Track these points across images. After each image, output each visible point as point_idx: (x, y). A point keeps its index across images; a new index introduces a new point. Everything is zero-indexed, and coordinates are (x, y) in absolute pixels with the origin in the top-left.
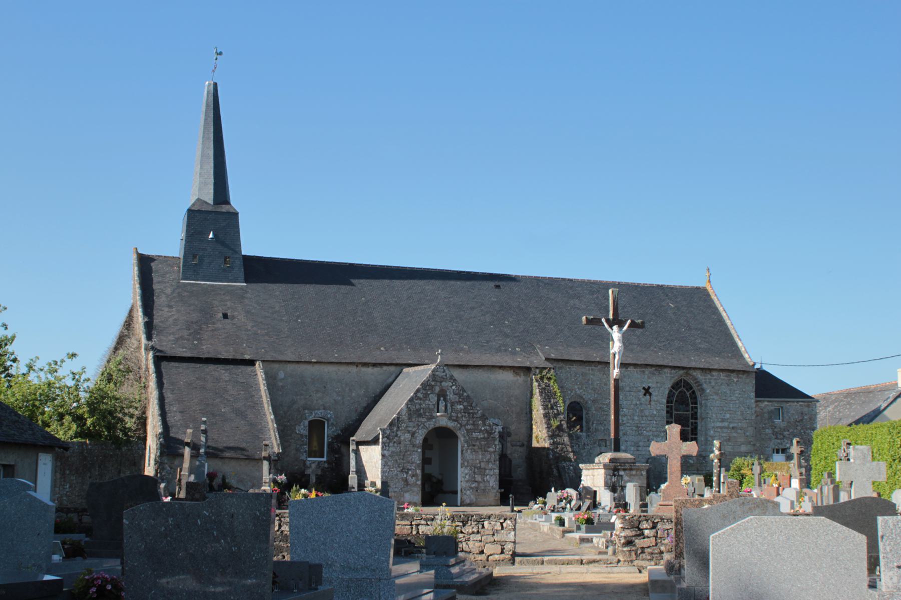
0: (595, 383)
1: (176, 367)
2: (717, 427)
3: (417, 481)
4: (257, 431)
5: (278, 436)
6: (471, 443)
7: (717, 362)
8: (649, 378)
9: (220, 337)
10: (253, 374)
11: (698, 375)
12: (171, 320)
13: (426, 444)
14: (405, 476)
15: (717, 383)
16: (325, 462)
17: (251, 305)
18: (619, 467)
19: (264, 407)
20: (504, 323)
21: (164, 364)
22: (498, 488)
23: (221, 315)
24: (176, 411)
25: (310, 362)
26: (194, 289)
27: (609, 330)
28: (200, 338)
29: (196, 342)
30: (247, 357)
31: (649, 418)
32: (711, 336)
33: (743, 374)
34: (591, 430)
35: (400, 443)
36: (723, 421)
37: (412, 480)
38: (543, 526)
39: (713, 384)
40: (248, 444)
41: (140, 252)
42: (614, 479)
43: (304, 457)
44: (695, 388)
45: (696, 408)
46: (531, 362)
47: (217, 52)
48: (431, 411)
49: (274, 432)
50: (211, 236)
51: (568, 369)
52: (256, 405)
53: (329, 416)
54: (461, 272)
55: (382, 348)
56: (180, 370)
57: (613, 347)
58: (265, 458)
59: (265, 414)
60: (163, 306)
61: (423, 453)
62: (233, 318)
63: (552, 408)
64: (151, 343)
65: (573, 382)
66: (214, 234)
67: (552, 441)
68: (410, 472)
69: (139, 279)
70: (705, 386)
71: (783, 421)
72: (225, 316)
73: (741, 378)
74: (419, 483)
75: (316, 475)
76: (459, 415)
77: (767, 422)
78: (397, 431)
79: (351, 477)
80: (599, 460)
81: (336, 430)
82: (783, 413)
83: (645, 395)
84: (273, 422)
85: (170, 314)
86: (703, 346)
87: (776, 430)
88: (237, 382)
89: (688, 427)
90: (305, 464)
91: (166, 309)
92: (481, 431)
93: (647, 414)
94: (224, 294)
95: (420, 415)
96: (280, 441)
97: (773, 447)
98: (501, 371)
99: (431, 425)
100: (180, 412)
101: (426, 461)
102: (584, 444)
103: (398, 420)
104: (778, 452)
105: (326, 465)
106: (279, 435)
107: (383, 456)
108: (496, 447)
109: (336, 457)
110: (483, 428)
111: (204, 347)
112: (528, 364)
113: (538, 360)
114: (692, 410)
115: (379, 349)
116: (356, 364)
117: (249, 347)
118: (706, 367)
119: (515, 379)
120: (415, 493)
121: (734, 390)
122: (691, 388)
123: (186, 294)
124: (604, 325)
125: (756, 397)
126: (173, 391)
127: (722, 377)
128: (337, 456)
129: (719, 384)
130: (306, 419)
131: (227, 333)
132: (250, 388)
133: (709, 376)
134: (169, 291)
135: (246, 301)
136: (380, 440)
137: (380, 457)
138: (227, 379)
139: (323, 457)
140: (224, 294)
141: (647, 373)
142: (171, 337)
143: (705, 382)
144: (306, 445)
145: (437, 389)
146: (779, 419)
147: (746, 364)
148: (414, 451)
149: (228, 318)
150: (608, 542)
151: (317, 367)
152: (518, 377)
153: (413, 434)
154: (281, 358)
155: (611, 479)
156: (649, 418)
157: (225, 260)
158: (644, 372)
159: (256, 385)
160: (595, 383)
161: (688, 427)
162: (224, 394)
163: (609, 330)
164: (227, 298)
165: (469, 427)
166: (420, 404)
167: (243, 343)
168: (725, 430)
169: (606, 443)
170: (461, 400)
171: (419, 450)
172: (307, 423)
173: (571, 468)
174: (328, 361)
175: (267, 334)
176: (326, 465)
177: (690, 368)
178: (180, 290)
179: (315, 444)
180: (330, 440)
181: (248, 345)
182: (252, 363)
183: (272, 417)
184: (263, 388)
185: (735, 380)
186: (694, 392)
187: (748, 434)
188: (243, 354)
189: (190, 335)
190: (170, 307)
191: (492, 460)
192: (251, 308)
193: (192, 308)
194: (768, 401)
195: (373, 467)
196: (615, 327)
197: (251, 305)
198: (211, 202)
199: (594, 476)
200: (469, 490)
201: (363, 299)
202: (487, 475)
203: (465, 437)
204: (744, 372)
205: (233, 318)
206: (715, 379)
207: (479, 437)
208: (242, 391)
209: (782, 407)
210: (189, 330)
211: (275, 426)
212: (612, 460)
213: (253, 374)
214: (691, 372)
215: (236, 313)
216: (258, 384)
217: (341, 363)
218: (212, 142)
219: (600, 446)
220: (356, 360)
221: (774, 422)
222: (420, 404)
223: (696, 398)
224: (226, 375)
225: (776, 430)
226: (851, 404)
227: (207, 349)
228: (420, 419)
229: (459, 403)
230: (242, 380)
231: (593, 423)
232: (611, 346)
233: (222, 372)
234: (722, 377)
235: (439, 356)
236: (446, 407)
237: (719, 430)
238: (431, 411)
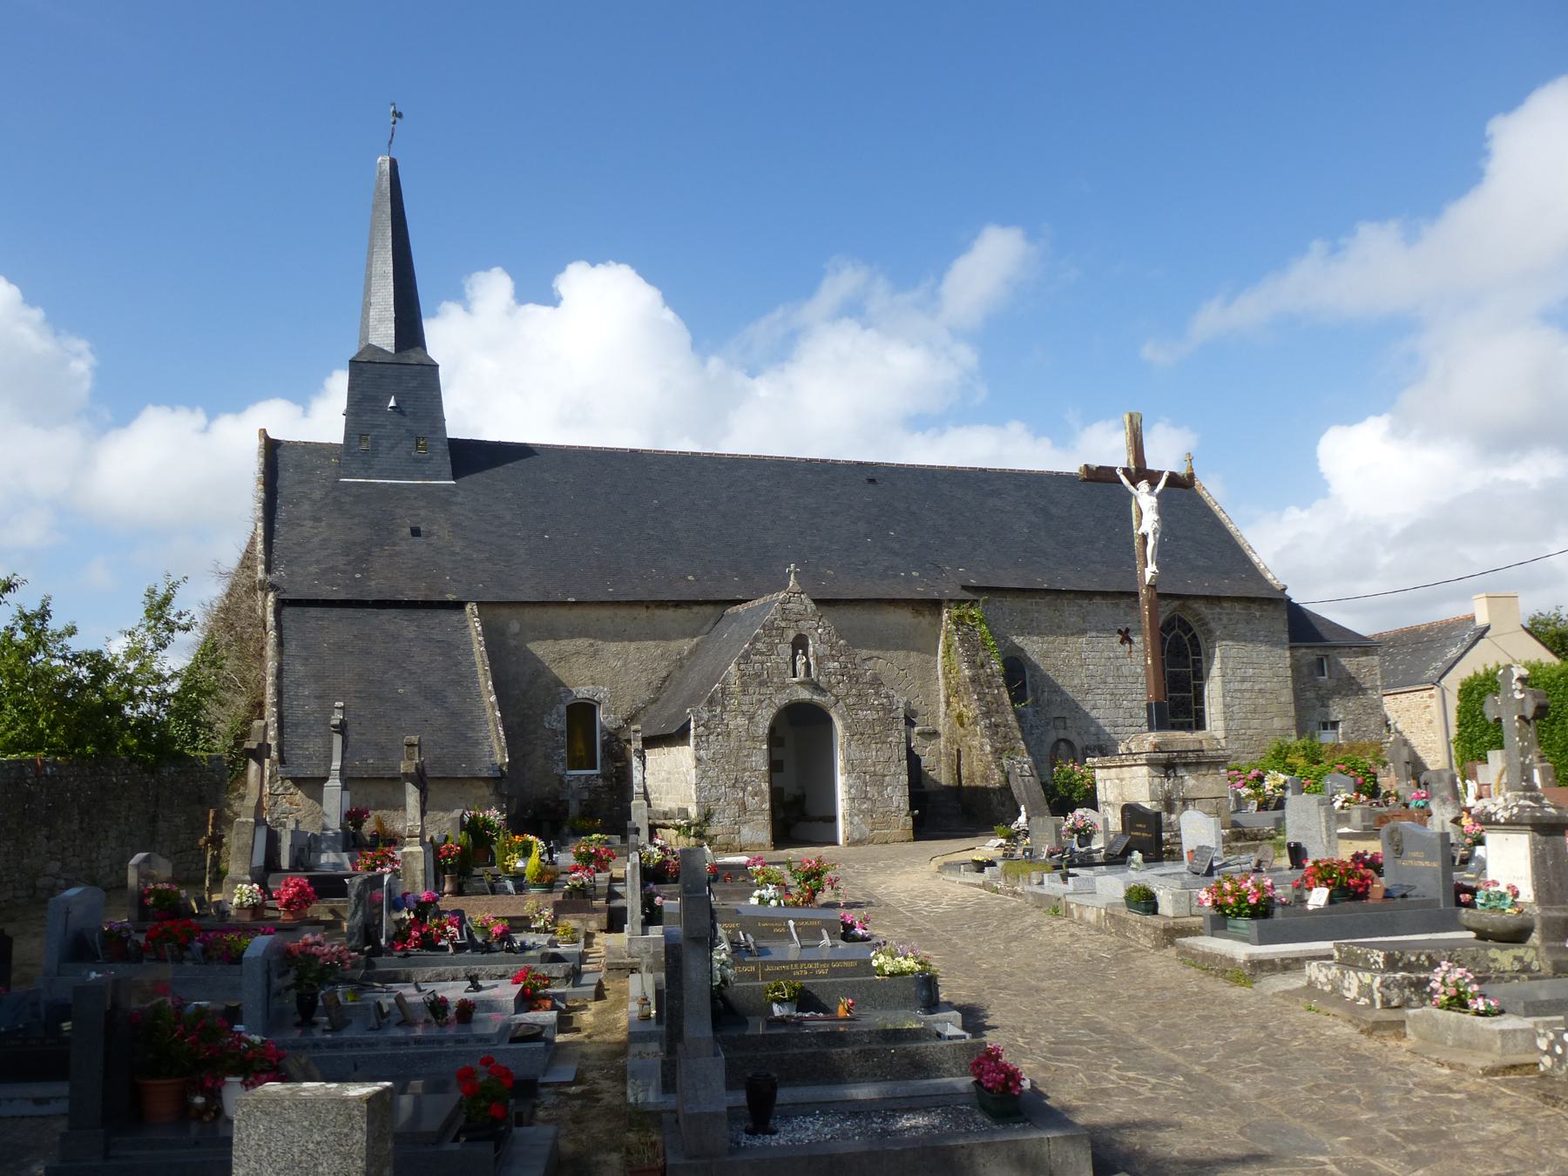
0: (1043, 626)
1: (318, 619)
2: (1235, 691)
3: (761, 805)
4: (462, 727)
5: (502, 733)
6: (853, 732)
7: (1227, 587)
8: (1126, 614)
9: (403, 566)
10: (460, 626)
11: (1201, 607)
12: (316, 540)
13: (774, 738)
14: (741, 794)
15: (1231, 620)
16: (598, 776)
17: (462, 515)
18: (1177, 761)
19: (478, 682)
20: (889, 535)
21: (288, 612)
22: (908, 808)
23: (408, 530)
24: (308, 697)
25: (564, 604)
26: (363, 491)
27: (1131, 488)
28: (366, 570)
29: (358, 576)
30: (451, 597)
31: (1130, 679)
32: (1210, 549)
33: (1269, 605)
34: (1040, 702)
35: (729, 735)
36: (1243, 681)
37: (752, 802)
38: (1078, 905)
39: (1225, 620)
40: (445, 751)
41: (272, 436)
42: (1168, 785)
43: (559, 770)
44: (1196, 630)
45: (1200, 661)
46: (941, 592)
47: (394, 112)
48: (781, 674)
49: (496, 725)
50: (392, 403)
51: (998, 604)
52: (464, 680)
53: (602, 695)
54: (811, 460)
55: (690, 578)
56: (325, 623)
57: (1140, 524)
58: (408, 777)
59: (479, 695)
60: (305, 519)
61: (770, 749)
62: (429, 534)
63: (982, 666)
64: (269, 579)
65: (1007, 624)
66: (396, 401)
67: (988, 721)
68: (750, 788)
69: (265, 477)
70: (1212, 625)
71: (1330, 678)
72: (416, 532)
73: (1265, 610)
74: (767, 806)
75: (581, 801)
76: (833, 680)
77: (1306, 680)
78: (722, 712)
79: (636, 805)
80: (1128, 748)
81: (616, 719)
82: (1329, 666)
83: (1122, 642)
84: (493, 708)
85: (316, 531)
86: (1201, 563)
87: (1320, 693)
88: (430, 640)
89: (1190, 692)
90: (561, 782)
91: (309, 523)
92: (872, 708)
93: (1126, 673)
94: (415, 498)
95: (762, 684)
96: (507, 742)
97: (1319, 719)
98: (892, 608)
99: (782, 700)
100: (316, 697)
101: (775, 766)
102: (1031, 726)
103: (723, 693)
104: (1325, 728)
105: (600, 782)
106: (505, 730)
107: (699, 760)
108: (897, 736)
109: (617, 767)
110: (876, 702)
111: (373, 583)
112: (936, 595)
113: (950, 590)
114: (1194, 664)
115: (685, 578)
116: (646, 604)
117: (455, 581)
118: (1213, 594)
119: (916, 620)
120: (761, 827)
121: (1258, 632)
122: (1190, 629)
123: (348, 499)
124: (1121, 482)
125: (1290, 641)
126: (307, 659)
127: (1237, 610)
128: (618, 765)
129: (1234, 622)
130: (561, 702)
131: (416, 559)
132: (454, 650)
133: (1218, 610)
134: (317, 495)
135: (455, 509)
136: (692, 732)
137: (692, 763)
138: (411, 636)
139: (594, 768)
140: (415, 498)
141: (1123, 606)
142: (313, 569)
143: (1214, 619)
144: (563, 747)
145: (791, 634)
146: (1324, 675)
147: (1271, 588)
148: (754, 748)
149: (420, 536)
150: (1387, 987)
151: (577, 611)
152: (921, 618)
153: (751, 718)
154: (512, 597)
155: (1162, 785)
156: (1130, 679)
157: (417, 444)
158: (1117, 605)
159: (466, 644)
160: (1043, 626)
161: (1190, 692)
162: (404, 662)
163: (1131, 488)
164: (421, 504)
165: (851, 701)
166: (762, 663)
167: (446, 575)
168: (1247, 695)
169: (1065, 723)
170: (834, 652)
171: (765, 747)
172: (563, 709)
173: (1026, 766)
174: (596, 599)
175: (488, 559)
176: (600, 782)
177: (1189, 597)
178: (337, 493)
179: (580, 745)
180: (605, 738)
181: (454, 577)
182: (459, 606)
183: (493, 698)
184: (479, 649)
185: (1258, 614)
186: (1194, 636)
187: (1283, 700)
188: (442, 593)
189: (349, 563)
190: (317, 519)
191: (895, 757)
192: (462, 518)
193: (356, 520)
194: (1307, 647)
195: (682, 782)
196: (1144, 485)
197: (462, 515)
198: (391, 348)
199: (1122, 780)
200: (858, 816)
201: (656, 501)
202: (887, 787)
203: (844, 719)
204: (1270, 601)
205: (429, 534)
206: (1228, 614)
207: (870, 718)
208: (440, 655)
209: (1327, 656)
210: (348, 555)
211: (498, 714)
212: (1158, 748)
213: (460, 626)
214: (1190, 603)
215: (435, 527)
216: (469, 643)
217: (618, 603)
218: (391, 252)
219: (1055, 728)
220: (645, 597)
221: (1317, 680)
222: (762, 663)
223: (1198, 645)
224: (411, 628)
225: (1320, 693)
226: (1392, 654)
227: (376, 588)
228: (763, 690)
229: (833, 658)
230: (440, 637)
231: (1043, 691)
232: (1135, 523)
233: (403, 625)
234: (1237, 610)
235: (792, 576)
236: (808, 665)
237: (1239, 695)
238: (781, 674)
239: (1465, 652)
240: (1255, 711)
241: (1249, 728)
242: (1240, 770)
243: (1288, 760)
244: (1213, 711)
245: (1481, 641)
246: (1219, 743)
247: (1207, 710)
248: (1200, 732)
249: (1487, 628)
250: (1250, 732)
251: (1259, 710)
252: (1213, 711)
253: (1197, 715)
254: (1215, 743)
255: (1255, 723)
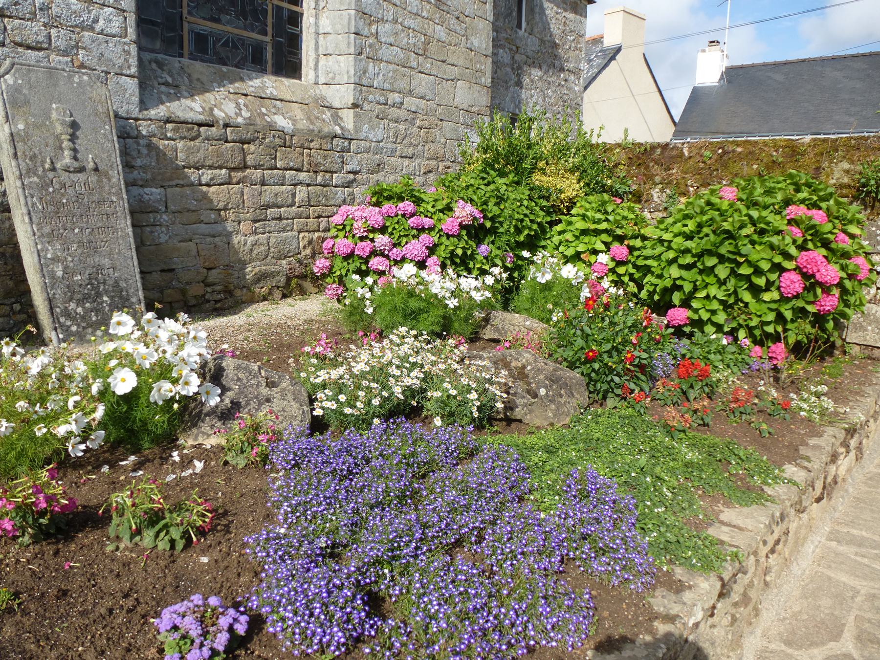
158: (84, 507)
239: (599, 72)
240: (423, 53)
241: (410, 93)
242: (418, 201)
243: (537, 179)
244: (325, 24)
245: (613, 62)
246: (336, 118)
247: (308, 21)
248: (287, 81)
249: (618, 50)
250: (411, 103)
251: (433, 48)
252: (325, 24)
253: (279, 30)
254: (327, 115)
255: (422, 84)
